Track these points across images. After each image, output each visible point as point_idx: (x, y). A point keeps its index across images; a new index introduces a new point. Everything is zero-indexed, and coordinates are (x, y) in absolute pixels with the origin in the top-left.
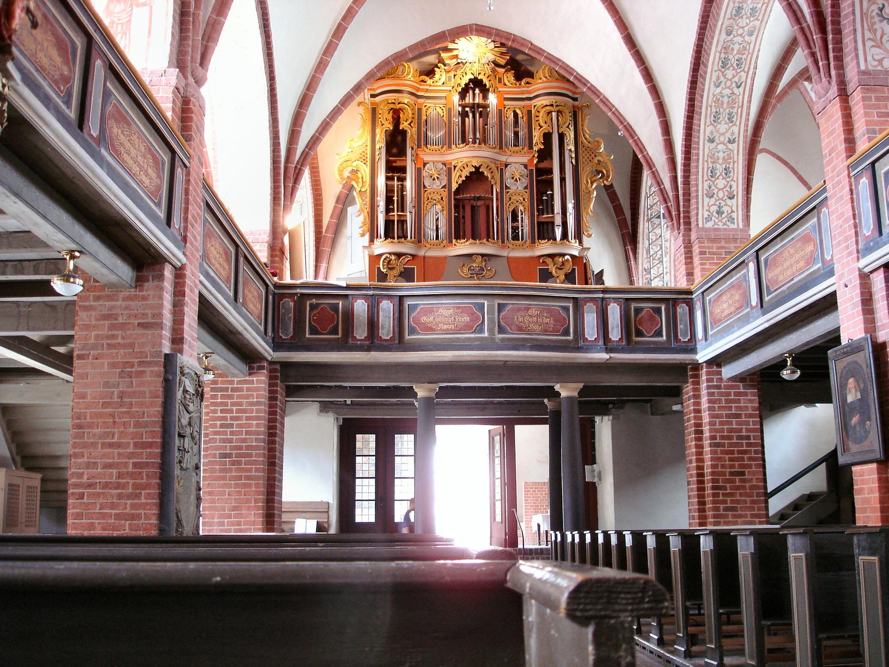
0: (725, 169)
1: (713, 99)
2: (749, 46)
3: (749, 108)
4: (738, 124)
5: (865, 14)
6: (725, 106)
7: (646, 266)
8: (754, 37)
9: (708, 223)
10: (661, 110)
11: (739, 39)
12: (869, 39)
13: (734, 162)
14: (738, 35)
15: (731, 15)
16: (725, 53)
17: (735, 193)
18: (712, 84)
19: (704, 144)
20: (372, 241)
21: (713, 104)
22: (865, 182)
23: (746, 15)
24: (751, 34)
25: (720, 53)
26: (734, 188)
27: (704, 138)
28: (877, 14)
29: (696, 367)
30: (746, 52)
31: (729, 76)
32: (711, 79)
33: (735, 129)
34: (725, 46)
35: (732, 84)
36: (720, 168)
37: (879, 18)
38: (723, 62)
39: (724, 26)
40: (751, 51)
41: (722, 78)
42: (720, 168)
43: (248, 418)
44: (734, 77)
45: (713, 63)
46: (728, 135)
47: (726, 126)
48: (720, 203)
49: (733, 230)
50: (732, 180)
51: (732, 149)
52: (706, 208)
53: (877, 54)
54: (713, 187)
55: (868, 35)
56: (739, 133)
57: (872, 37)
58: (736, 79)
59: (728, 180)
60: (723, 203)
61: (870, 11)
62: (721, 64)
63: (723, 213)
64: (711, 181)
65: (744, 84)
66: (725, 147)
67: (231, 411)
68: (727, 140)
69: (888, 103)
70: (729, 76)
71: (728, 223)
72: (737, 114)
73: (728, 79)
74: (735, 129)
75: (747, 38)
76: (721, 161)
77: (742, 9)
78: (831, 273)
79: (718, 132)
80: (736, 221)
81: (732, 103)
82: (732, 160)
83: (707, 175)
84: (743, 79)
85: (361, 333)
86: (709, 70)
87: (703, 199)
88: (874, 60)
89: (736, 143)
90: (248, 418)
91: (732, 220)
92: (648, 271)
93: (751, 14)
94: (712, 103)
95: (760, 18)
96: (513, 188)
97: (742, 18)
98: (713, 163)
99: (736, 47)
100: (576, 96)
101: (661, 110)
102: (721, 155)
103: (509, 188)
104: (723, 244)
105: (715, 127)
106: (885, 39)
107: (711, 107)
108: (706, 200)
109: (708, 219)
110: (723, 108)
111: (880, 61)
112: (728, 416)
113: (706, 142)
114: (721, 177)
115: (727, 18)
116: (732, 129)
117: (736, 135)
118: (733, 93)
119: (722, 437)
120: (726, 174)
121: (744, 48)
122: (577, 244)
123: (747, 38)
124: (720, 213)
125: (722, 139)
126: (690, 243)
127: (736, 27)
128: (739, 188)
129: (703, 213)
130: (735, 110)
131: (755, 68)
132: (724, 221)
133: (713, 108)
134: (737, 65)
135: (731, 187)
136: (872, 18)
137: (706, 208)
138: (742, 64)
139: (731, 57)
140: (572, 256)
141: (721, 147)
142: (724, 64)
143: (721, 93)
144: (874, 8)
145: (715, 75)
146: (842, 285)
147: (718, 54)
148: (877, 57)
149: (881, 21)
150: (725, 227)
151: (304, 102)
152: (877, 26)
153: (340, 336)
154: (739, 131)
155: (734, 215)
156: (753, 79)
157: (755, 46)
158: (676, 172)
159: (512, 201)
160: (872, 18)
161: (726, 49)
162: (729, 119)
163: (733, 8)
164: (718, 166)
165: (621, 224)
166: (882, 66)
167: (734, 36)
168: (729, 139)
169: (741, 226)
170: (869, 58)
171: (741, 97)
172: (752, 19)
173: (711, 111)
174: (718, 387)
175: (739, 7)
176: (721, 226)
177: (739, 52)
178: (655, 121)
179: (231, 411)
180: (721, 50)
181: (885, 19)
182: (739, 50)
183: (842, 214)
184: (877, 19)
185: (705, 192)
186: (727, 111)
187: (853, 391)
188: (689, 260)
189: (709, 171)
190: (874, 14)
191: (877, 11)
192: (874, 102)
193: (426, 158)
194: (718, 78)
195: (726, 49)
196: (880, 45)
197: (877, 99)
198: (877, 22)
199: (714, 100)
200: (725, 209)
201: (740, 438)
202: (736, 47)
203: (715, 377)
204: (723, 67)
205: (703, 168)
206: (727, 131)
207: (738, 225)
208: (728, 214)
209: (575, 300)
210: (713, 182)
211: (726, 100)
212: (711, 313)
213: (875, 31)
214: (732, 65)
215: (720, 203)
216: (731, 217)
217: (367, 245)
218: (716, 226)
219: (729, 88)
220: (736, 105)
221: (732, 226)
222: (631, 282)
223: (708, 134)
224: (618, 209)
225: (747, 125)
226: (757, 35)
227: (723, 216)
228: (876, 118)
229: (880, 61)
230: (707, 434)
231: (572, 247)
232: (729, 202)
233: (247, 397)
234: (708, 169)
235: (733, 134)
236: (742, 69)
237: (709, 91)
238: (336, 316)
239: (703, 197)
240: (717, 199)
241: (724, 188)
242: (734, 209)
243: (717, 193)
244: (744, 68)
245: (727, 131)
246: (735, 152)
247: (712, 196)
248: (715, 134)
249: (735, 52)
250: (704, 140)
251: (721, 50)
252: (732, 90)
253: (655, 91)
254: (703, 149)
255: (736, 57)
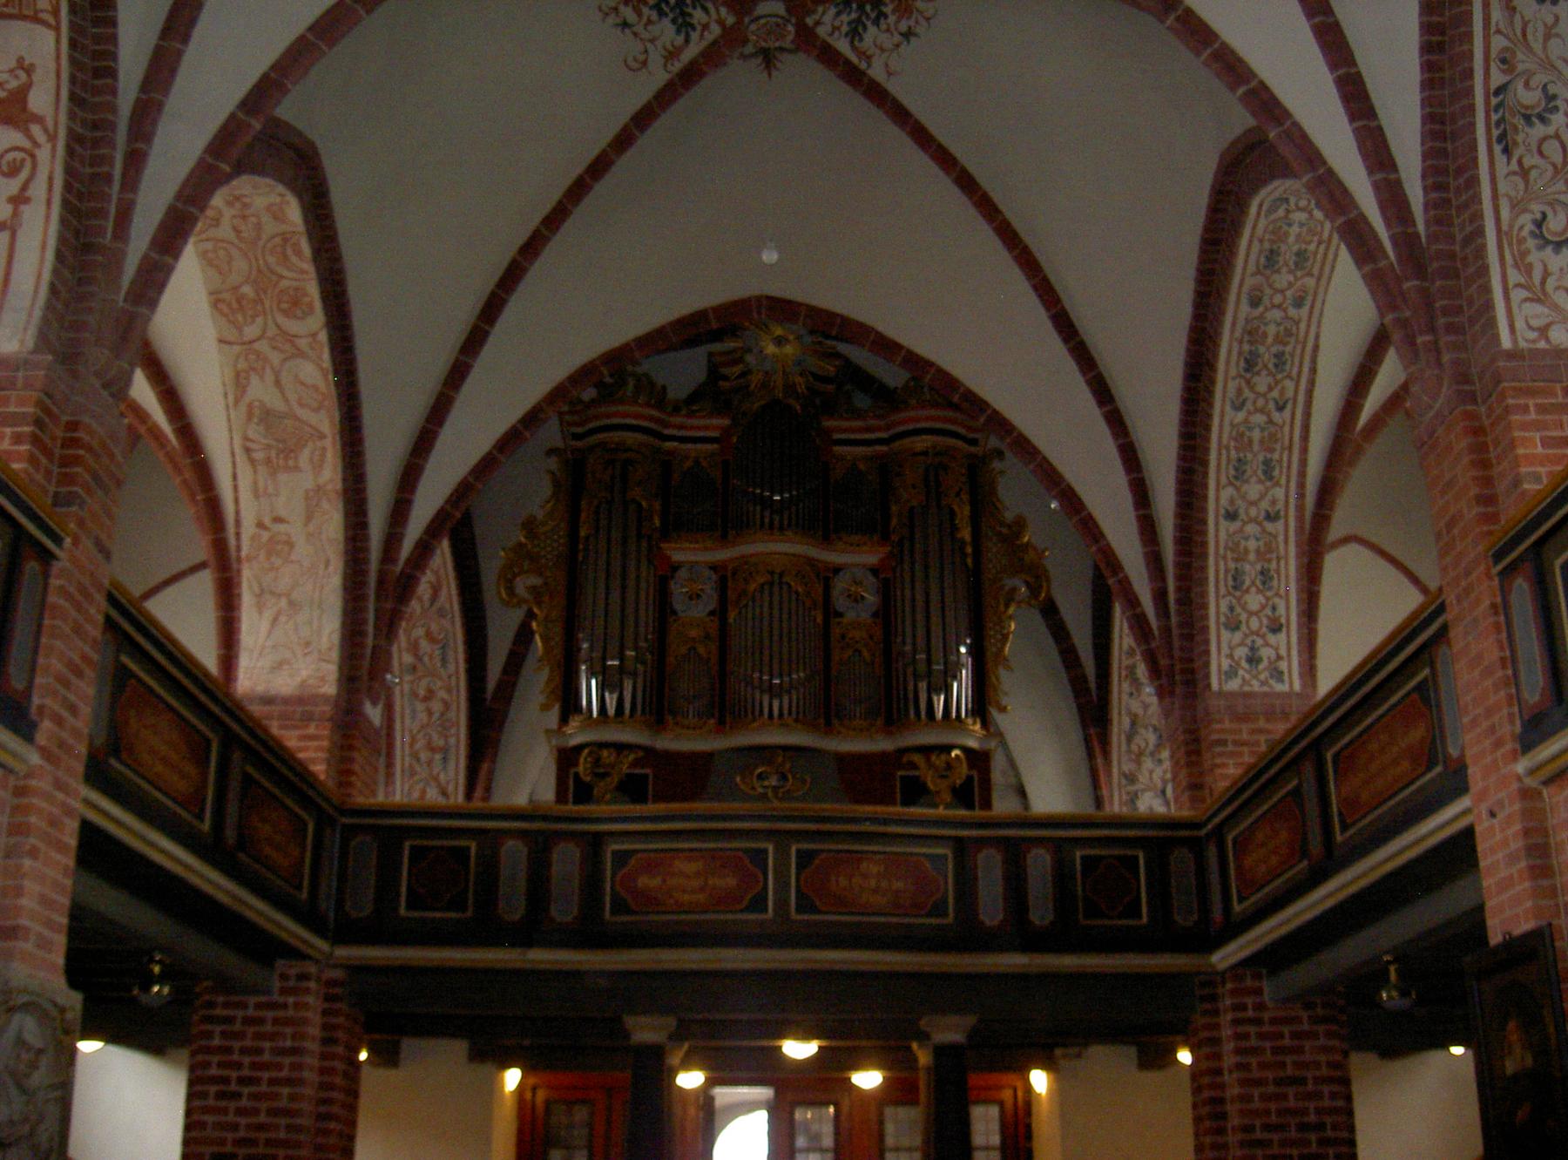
0: (1262, 573)
1: (1231, 433)
2: (1298, 329)
3: (1304, 450)
4: (1283, 481)
5: (1506, 234)
6: (1256, 447)
7: (1126, 768)
8: (1305, 311)
9: (1230, 683)
10: (1130, 457)
11: (1276, 314)
12: (1518, 285)
13: (1278, 559)
14: (1274, 306)
15: (1258, 267)
16: (1251, 343)
17: (1283, 620)
18: (1228, 403)
19: (1217, 524)
20: (564, 720)
21: (1232, 444)
22: (1522, 587)
23: (1287, 265)
24: (1299, 303)
25: (1241, 342)
26: (1281, 610)
27: (1217, 510)
28: (1532, 233)
29: (1212, 980)
30: (1292, 340)
31: (1262, 388)
32: (1224, 392)
33: (1279, 493)
34: (1249, 328)
35: (1267, 402)
36: (1250, 571)
37: (1536, 241)
38: (1247, 361)
39: (1245, 289)
40: (1302, 334)
41: (1247, 393)
42: (1250, 571)
43: (272, 1082)
44: (1270, 389)
45: (1228, 362)
46: (1264, 505)
47: (1260, 487)
48: (1253, 641)
49: (1279, 695)
50: (1277, 595)
51: (1274, 532)
52: (1225, 650)
53: (1537, 316)
54: (1238, 610)
55: (1514, 276)
56: (1287, 502)
57: (1523, 281)
58: (1275, 394)
59: (1269, 594)
60: (1259, 642)
61: (1516, 228)
62: (1242, 364)
63: (1259, 660)
64: (1234, 596)
65: (1290, 402)
66: (1259, 529)
67: (239, 1066)
68: (1263, 514)
69: (1565, 418)
70: (1262, 388)
71: (1272, 682)
72: (1280, 461)
73: (1258, 394)
74: (1279, 493)
75: (1292, 312)
76: (1252, 557)
77: (1279, 255)
78: (1461, 788)
79: (1243, 498)
80: (1286, 677)
81: (1269, 443)
82: (1274, 555)
83: (1226, 586)
84: (1290, 393)
85: (513, 906)
86: (1220, 378)
87: (1219, 637)
88: (1530, 328)
89: (1282, 521)
90: (272, 1082)
91: (1278, 675)
92: (1131, 778)
93: (1296, 264)
94: (1229, 442)
95: (1316, 271)
96: (850, 616)
97: (1278, 271)
98: (1236, 560)
99: (1272, 330)
100: (972, 435)
101: (1130, 457)
102: (1252, 545)
103: (841, 615)
104: (1262, 723)
105: (1238, 489)
106: (1551, 283)
107: (1228, 448)
108: (1225, 635)
109: (1232, 673)
110: (1252, 451)
111: (1543, 331)
112: (1279, 1082)
113: (1222, 520)
114: (1253, 589)
115: (1249, 272)
116: (1270, 493)
117: (1280, 505)
118: (1270, 421)
119: (1267, 1127)
120: (1264, 583)
121: (1288, 333)
122: (978, 727)
123: (1292, 312)
124: (1253, 660)
125: (1253, 512)
126: (1195, 722)
127: (1268, 291)
128: (1290, 610)
129: (1217, 663)
130: (1276, 456)
131: (1313, 370)
132: (1262, 677)
133: (1233, 453)
134: (1276, 366)
135: (1274, 608)
136: (1521, 241)
137: (1225, 650)
138: (1284, 363)
139: (1262, 349)
140: (965, 750)
141: (1251, 529)
142: (1250, 364)
143: (1246, 421)
144: (1526, 220)
145: (1232, 386)
146: (1484, 815)
147: (1236, 346)
148: (1535, 323)
149: (1541, 248)
150: (1266, 689)
151: (423, 443)
152: (1534, 258)
153: (469, 913)
154: (1287, 496)
155: (1283, 665)
156: (1310, 393)
157: (1309, 326)
158: (1164, 579)
159: (847, 640)
160: (1521, 241)
161: (1253, 333)
162: (1265, 472)
163: (1261, 252)
164: (1247, 567)
165: (1078, 683)
166: (1548, 340)
167: (1266, 309)
168: (1267, 512)
169: (1297, 686)
170: (1520, 324)
171: (1287, 429)
172: (1299, 274)
173: (1228, 457)
174: (1258, 1021)
175: (1272, 251)
176: (1256, 686)
177: (1278, 340)
178: (1119, 478)
179: (239, 1066)
180: (1243, 337)
181: (1548, 242)
182: (1277, 336)
183: (1480, 656)
184: (1531, 243)
185: (1223, 619)
186: (1261, 458)
187: (1518, 1050)
188: (1194, 758)
189: (1230, 578)
190: (1525, 233)
191: (1529, 227)
192: (1533, 416)
193: (677, 557)
194: (1239, 391)
195: (1253, 333)
196: (1540, 297)
197: (1541, 409)
198: (1533, 250)
199: (1234, 433)
200: (1266, 653)
201: (1302, 1127)
202: (1272, 330)
203: (1249, 1001)
204: (1247, 370)
205: (1217, 571)
206: (1262, 497)
207: (1291, 684)
208: (1270, 663)
209: (958, 841)
210: (1239, 599)
211: (1256, 435)
212: (1239, 868)
213: (1528, 270)
214: (1265, 366)
215: (1253, 641)
216: (1276, 669)
217: (555, 726)
218: (1246, 688)
219: (1262, 411)
220: (1278, 447)
221: (1282, 688)
222: (1099, 802)
223: (1224, 502)
224: (1069, 656)
225: (1301, 485)
226: (1312, 307)
227: (1261, 667)
228: (1540, 450)
229: (1543, 331)
230: (1235, 1121)
231: (970, 733)
232: (1272, 638)
233: (272, 1037)
234: (1227, 571)
235: (1274, 502)
236: (1285, 374)
237: (1223, 419)
238: (639, 855)
239: (1218, 630)
240: (1247, 632)
241: (1260, 611)
242: (1283, 652)
243: (1247, 622)
244: (1291, 370)
245: (1262, 497)
246: (1281, 538)
247: (1237, 628)
248: (1239, 502)
249: (1270, 340)
250: (1217, 517)
251: (1243, 337)
252: (1268, 415)
253: (1116, 421)
254: (1217, 532)
255: (1274, 350)
